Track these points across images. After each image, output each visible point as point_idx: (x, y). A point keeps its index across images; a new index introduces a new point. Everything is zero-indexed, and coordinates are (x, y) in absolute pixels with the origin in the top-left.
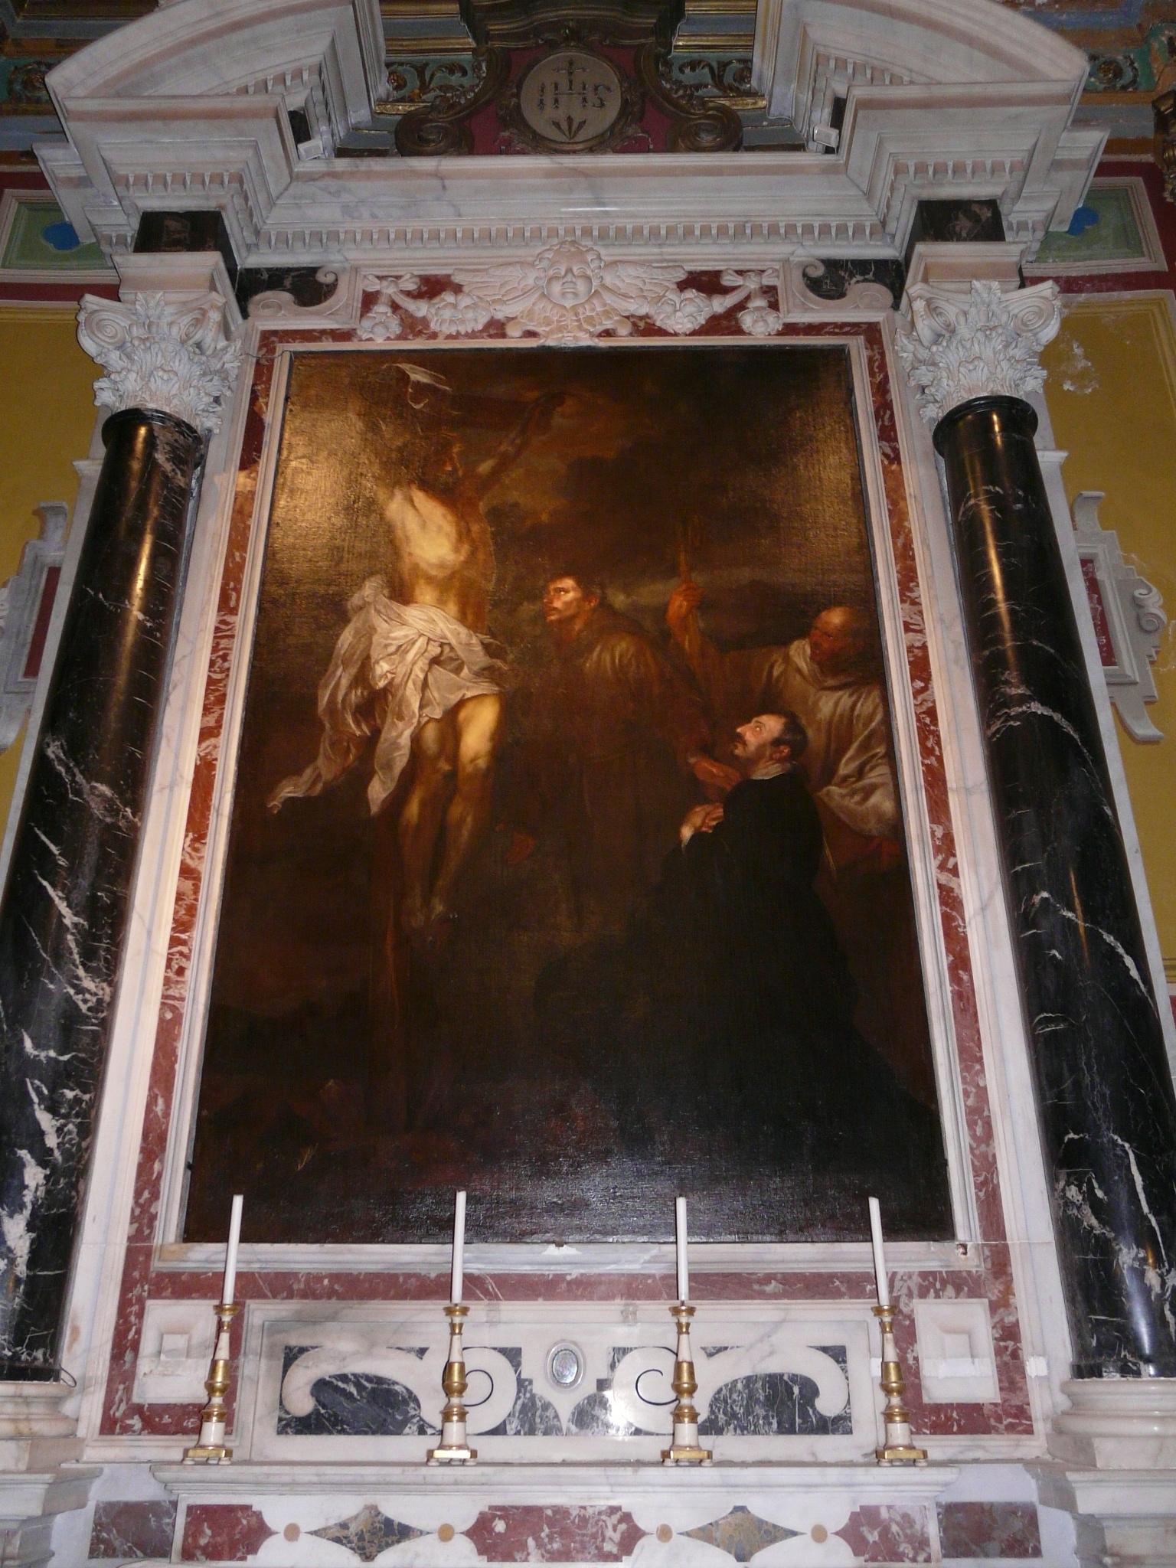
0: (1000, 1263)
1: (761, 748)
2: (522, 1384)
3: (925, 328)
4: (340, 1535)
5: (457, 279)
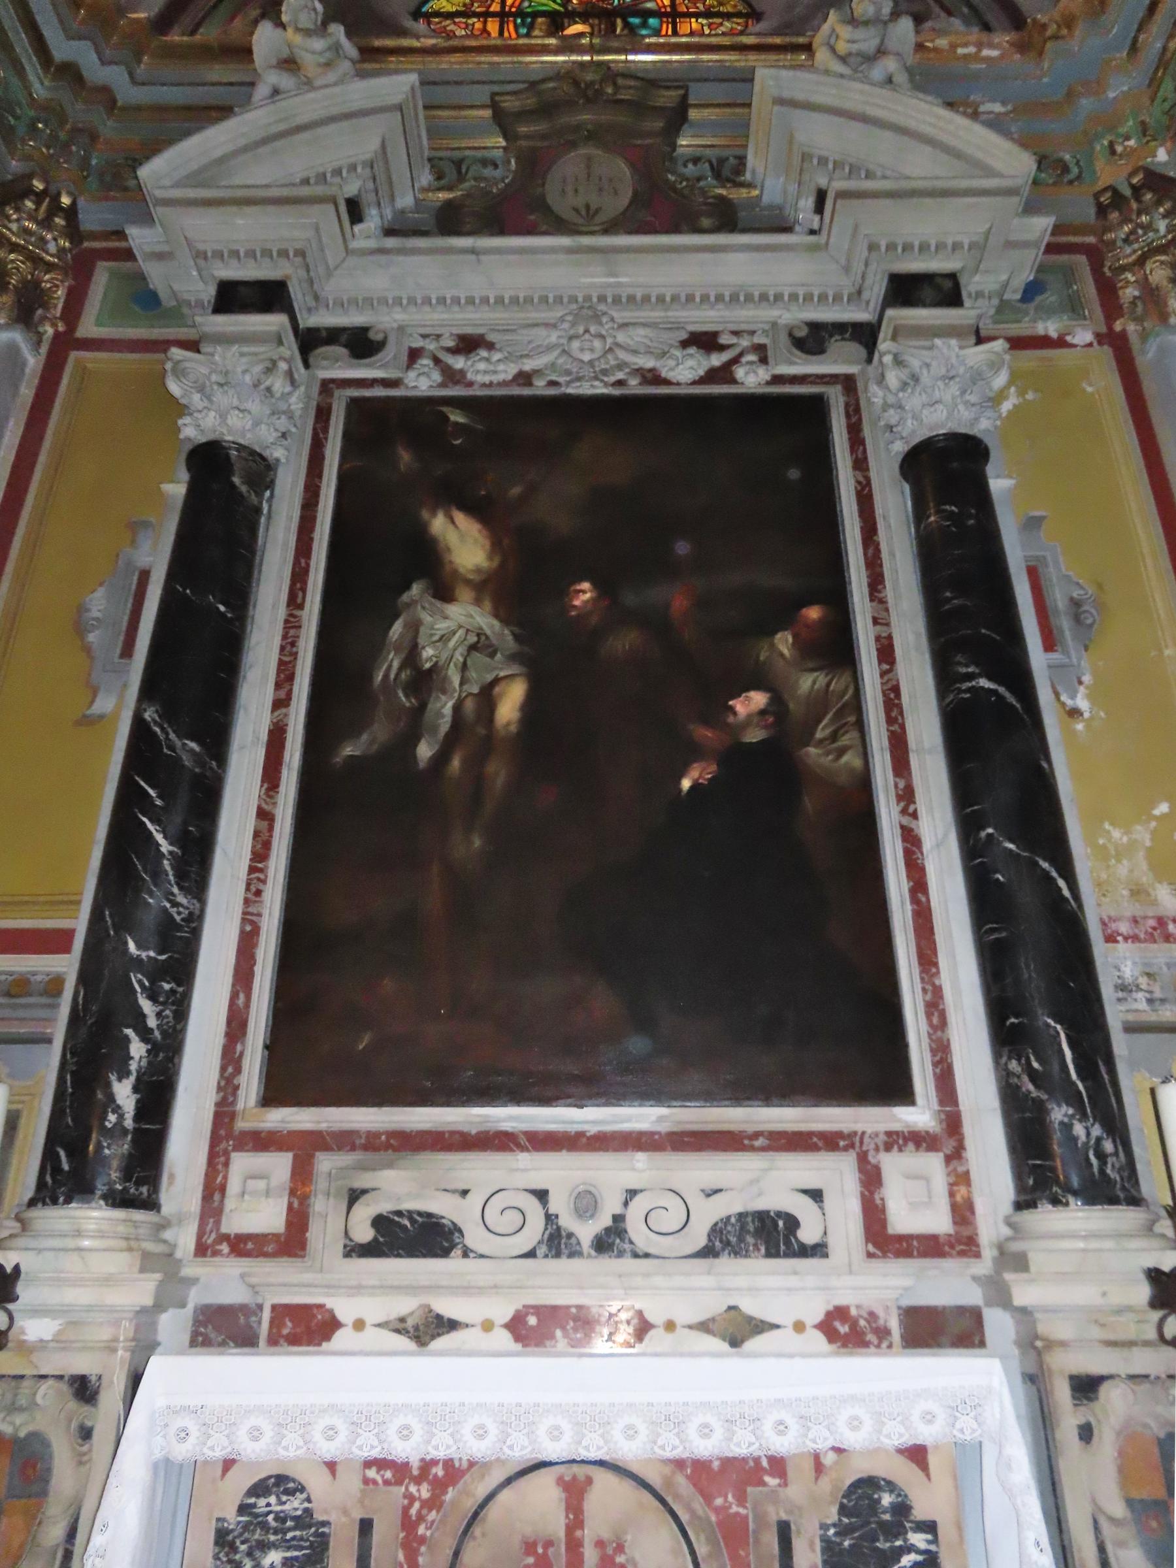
0: (953, 1124)
1: (750, 716)
2: (550, 1218)
3: (893, 378)
4: (399, 1327)
5: (491, 337)
